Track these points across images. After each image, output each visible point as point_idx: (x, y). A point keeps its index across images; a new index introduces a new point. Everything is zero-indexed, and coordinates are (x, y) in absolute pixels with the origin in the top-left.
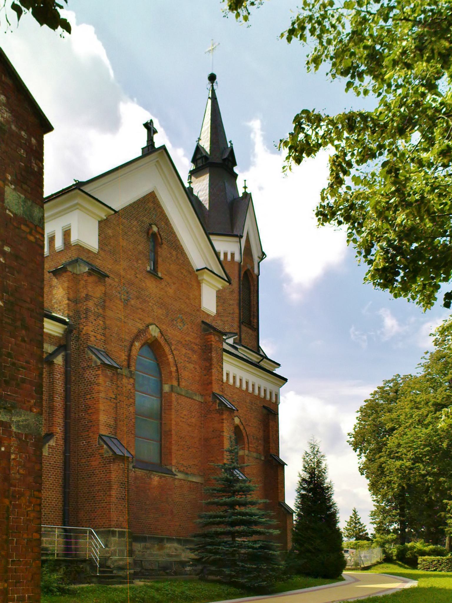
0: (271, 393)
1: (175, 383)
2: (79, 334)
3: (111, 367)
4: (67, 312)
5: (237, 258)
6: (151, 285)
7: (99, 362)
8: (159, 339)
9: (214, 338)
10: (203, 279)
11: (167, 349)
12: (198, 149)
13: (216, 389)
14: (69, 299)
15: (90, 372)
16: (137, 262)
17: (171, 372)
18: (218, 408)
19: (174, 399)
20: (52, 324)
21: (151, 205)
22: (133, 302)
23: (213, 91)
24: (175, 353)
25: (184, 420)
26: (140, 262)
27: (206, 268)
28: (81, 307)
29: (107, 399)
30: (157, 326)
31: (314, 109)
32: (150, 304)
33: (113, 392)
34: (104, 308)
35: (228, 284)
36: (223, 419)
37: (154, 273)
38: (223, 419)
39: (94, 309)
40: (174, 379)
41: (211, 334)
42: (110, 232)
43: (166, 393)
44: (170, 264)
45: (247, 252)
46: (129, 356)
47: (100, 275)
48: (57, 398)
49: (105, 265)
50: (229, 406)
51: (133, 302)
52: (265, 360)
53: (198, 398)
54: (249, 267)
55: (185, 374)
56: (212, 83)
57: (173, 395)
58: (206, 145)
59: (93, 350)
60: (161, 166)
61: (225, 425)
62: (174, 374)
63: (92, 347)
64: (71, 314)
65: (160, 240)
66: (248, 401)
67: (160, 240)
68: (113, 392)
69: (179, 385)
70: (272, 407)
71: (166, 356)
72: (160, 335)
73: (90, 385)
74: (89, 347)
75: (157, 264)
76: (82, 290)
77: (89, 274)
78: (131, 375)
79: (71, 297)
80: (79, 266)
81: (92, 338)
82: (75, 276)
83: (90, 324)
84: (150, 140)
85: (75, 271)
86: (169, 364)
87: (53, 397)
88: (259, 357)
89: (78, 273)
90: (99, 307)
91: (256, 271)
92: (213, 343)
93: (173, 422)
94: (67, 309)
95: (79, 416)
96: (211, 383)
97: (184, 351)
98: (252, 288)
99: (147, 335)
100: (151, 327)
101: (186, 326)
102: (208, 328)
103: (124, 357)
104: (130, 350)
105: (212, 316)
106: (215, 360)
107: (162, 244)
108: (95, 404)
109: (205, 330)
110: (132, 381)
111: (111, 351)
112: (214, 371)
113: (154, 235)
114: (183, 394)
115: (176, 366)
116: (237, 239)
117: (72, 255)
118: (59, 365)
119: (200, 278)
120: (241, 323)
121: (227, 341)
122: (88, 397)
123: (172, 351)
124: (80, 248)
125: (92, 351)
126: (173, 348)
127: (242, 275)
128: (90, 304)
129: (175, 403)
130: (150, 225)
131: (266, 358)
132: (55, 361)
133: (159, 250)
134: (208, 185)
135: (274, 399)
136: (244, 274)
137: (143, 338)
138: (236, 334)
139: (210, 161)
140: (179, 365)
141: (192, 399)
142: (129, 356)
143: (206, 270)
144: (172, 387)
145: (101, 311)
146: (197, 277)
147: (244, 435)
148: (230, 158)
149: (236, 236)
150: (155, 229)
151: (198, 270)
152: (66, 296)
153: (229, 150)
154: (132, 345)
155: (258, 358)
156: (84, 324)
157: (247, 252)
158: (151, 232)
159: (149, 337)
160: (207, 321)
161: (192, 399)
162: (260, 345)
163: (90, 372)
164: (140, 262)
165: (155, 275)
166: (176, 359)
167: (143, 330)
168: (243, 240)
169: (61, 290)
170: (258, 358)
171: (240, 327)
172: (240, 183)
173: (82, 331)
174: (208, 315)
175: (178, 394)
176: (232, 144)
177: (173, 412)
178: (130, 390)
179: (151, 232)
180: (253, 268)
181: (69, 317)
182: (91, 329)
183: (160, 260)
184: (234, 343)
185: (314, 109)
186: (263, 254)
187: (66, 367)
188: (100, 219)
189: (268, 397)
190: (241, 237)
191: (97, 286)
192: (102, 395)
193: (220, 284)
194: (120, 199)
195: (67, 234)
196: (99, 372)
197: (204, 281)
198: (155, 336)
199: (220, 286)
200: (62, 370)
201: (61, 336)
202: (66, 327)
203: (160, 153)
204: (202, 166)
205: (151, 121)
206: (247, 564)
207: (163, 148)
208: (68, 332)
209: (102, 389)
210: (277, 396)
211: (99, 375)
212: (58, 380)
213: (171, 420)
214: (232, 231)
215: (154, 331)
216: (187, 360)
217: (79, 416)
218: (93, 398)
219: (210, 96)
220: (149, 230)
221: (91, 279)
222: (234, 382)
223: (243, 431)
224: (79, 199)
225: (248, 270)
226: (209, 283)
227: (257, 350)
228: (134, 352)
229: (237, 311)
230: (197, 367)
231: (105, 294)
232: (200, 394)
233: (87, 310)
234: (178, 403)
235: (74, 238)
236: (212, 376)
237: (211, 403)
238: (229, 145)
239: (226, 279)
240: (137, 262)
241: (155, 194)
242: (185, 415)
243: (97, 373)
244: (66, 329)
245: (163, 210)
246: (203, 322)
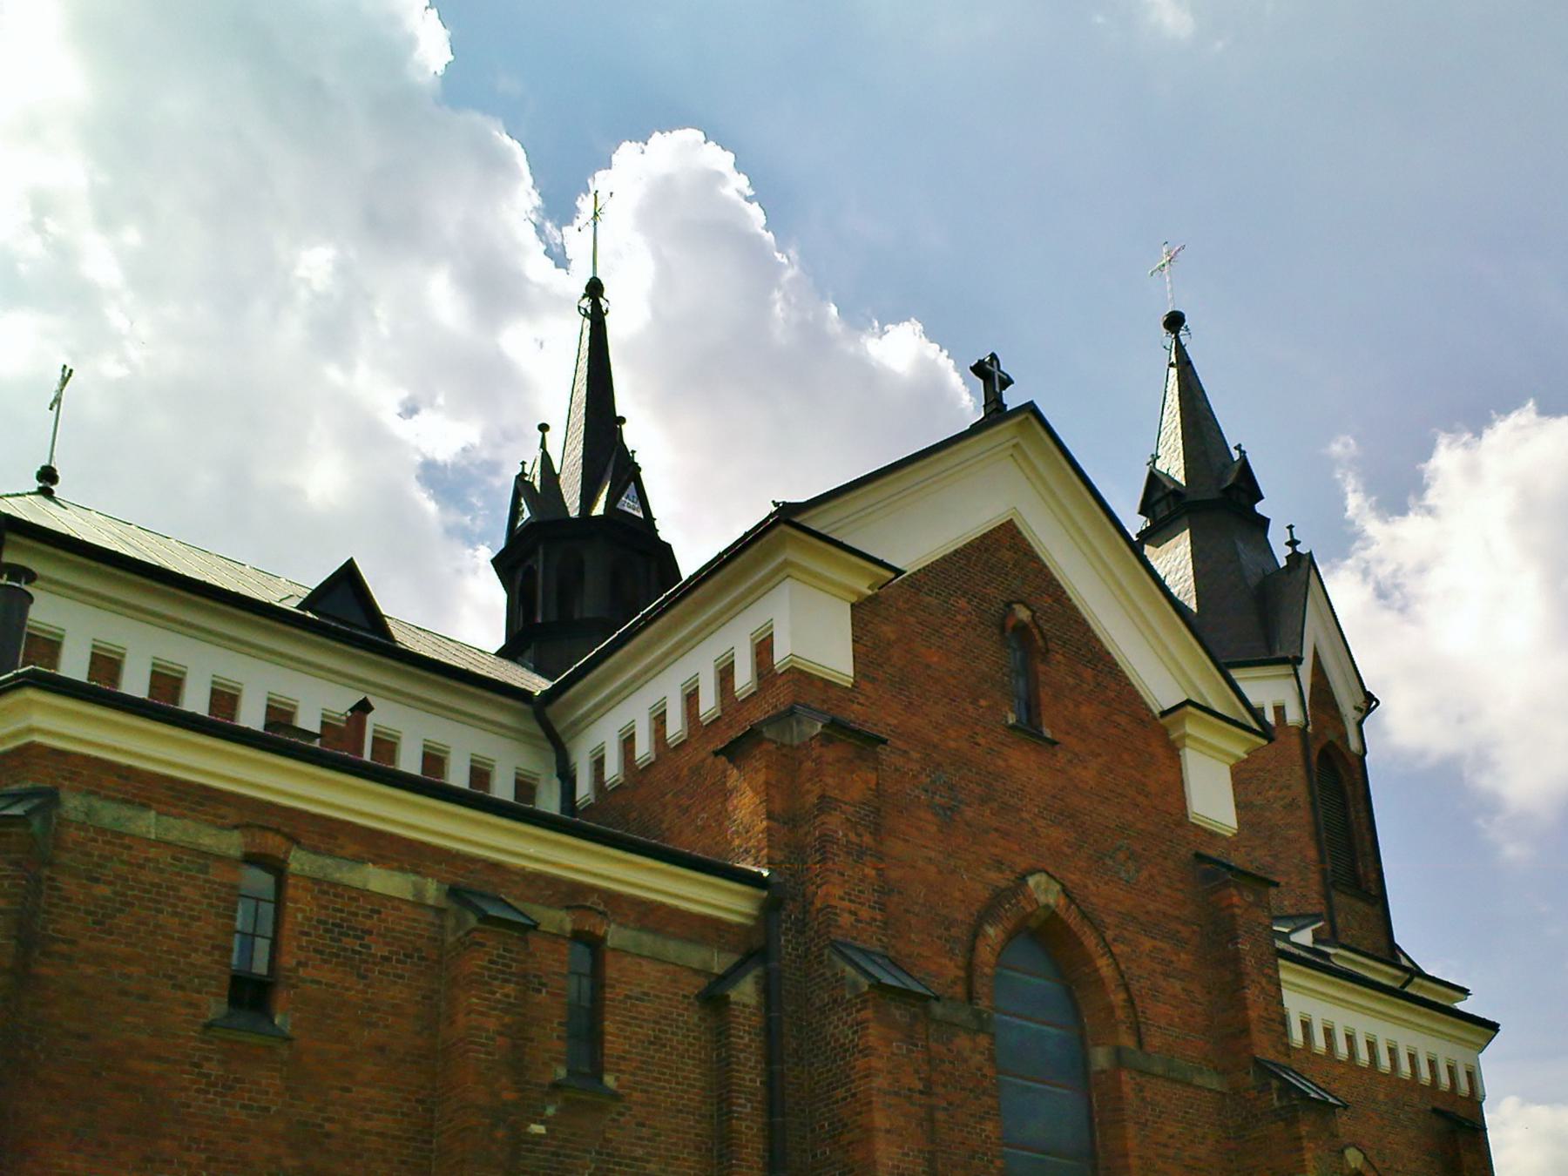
0: (1451, 1070)
1: (1127, 1041)
2: (806, 912)
3: (904, 994)
4: (765, 851)
5: (1294, 716)
6: (1022, 763)
7: (864, 984)
8: (1062, 914)
9: (1239, 899)
10: (1185, 736)
11: (1090, 941)
12: (1154, 480)
13: (1265, 1049)
14: (770, 816)
15: (840, 1019)
16: (975, 702)
17: (1110, 1009)
18: (1276, 1104)
19: (1126, 1089)
20: (730, 891)
21: (1006, 555)
22: (969, 813)
23: (1180, 349)
24: (1118, 949)
25: (1171, 1152)
26: (983, 703)
27: (1188, 702)
28: (806, 834)
29: (897, 1094)
30: (1051, 876)
32: (1024, 815)
33: (916, 1072)
34: (877, 830)
35: (1264, 742)
36: (1300, 1138)
37: (1029, 730)
38: (1300, 1138)
39: (846, 835)
40: (1123, 1028)
41: (1226, 884)
42: (889, 631)
43: (1103, 1071)
44: (1077, 705)
45: (1322, 697)
46: (970, 967)
47: (867, 742)
48: (740, 1105)
49: (880, 716)
50: (1313, 1095)
51: (969, 813)
52: (1416, 980)
53: (1213, 1082)
54: (1331, 735)
56: (1176, 332)
57: (1125, 1076)
58: (1173, 465)
59: (849, 952)
60: (1026, 457)
61: (1308, 1156)
63: (846, 945)
64: (779, 856)
65: (1041, 643)
66: (1381, 1097)
67: (1041, 643)
68: (916, 1072)
69: (1140, 1043)
70: (1462, 1112)
71: (1088, 960)
72: (1063, 901)
73: (843, 1058)
74: (834, 945)
75: (1038, 705)
76: (808, 785)
77: (826, 739)
78: (982, 1025)
79: (778, 806)
80: (799, 722)
81: (846, 919)
82: (784, 751)
83: (835, 878)
85: (787, 740)
86: (1100, 982)
87: (732, 1104)
88: (1399, 973)
89: (796, 742)
90: (860, 829)
91: (1354, 744)
92: (1237, 911)
93: (1133, 1161)
94: (764, 843)
95: (814, 1156)
96: (1245, 1031)
97: (1148, 944)
98: (1349, 789)
99: (1023, 903)
100: (1031, 881)
101: (1145, 874)
102: (1210, 867)
103: (952, 969)
104: (972, 949)
105: (1224, 837)
106: (1250, 963)
107: (1048, 651)
108: (859, 1113)
110: (983, 1041)
111: (909, 956)
112: (1251, 993)
113: (1022, 630)
114: (1159, 1069)
115: (1127, 989)
116: (1288, 669)
117: (781, 698)
118: (745, 1006)
119: (1174, 735)
120: (1329, 886)
121: (1295, 938)
122: (841, 1093)
123: (1106, 945)
124: (800, 677)
125: (841, 952)
126: (1109, 935)
127: (1314, 757)
128: (834, 822)
130: (1009, 605)
131: (1419, 973)
132: (734, 995)
133: (1041, 667)
134: (1189, 555)
135: (1464, 1087)
136: (1319, 757)
138: (1316, 917)
139: (1188, 499)
140: (1135, 986)
141: (1189, 1084)
142: (970, 967)
143: (1190, 709)
144: (1118, 1052)
145: (868, 839)
146: (1164, 732)
148: (1243, 485)
149: (1283, 661)
150: (1023, 614)
151: (1164, 713)
152: (762, 809)
153: (1237, 467)
154: (976, 933)
155: (1395, 978)
156: (819, 881)
157: (1322, 697)
158: (1010, 623)
159: (1029, 909)
160: (1213, 854)
161: (1189, 1084)
162: (1397, 941)
163: (840, 1019)
164: (983, 703)
165: (1032, 735)
166: (1123, 967)
167: (1009, 889)
168: (1305, 670)
169: (749, 793)
170: (1395, 978)
172: (1277, 539)
173: (812, 903)
174: (1213, 835)
175: (1142, 1072)
176: (1243, 453)
177: (1131, 1130)
178: (979, 1069)
179: (1010, 623)
180: (1344, 737)
181: (770, 864)
182: (840, 894)
183: (1045, 695)
184: (1316, 940)
186: (1370, 698)
187: (768, 1009)
188: (854, 599)
189: (1444, 1080)
190: (1298, 660)
191: (853, 772)
192: (879, 1082)
193: (1238, 746)
194: (915, 540)
195: (763, 648)
196: (868, 1013)
197: (1188, 742)
198: (1047, 906)
199: (1240, 752)
200: (757, 1021)
201: (749, 922)
202: (765, 894)
203: (1020, 423)
204: (1170, 515)
205: (993, 356)
207: (1030, 409)
208: (771, 908)
209: (876, 1063)
210: (1472, 1076)
211: (867, 1020)
212: (742, 1051)
213: (1126, 1155)
214: (1270, 648)
215: (1043, 891)
216: (1158, 968)
217: (814, 1156)
218: (854, 1095)
219: (1174, 360)
220: (1004, 617)
221: (830, 754)
224: (794, 552)
225: (1331, 744)
226: (1203, 742)
227: (1391, 953)
228: (985, 954)
229: (1312, 854)
231: (879, 792)
232: (1215, 1068)
233: (825, 840)
234: (1143, 1099)
235: (781, 654)
236: (1246, 1008)
237: (1254, 1093)
238: (1236, 455)
239: (1255, 726)
240: (975, 702)
241: (1015, 527)
242: (1172, 1137)
243: (860, 1016)
244: (766, 899)
245: (1045, 566)
246: (1200, 857)
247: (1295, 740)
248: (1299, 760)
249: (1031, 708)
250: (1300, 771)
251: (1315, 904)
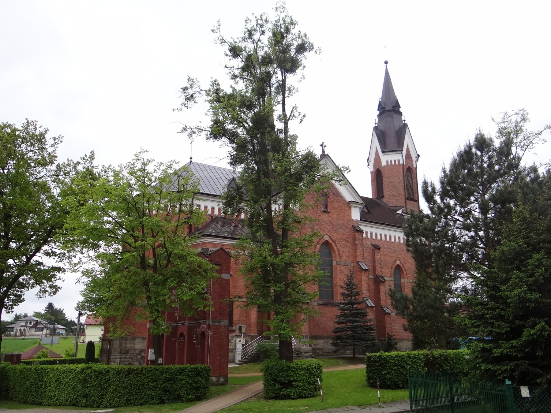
1: (338, 260)
11: (333, 244)
31: (389, 108)
37: (326, 212)
54: (409, 165)
55: (343, 254)
62: (337, 256)
84: (323, 151)
91: (415, 166)
93: (338, 279)
97: (343, 243)
109: (353, 230)
115: (338, 251)
127: (405, 171)
129: (338, 269)
137: (321, 243)
147: (404, 270)
157: (408, 156)
168: (404, 152)
171: (405, 202)
180: (412, 165)
184: (402, 212)
185: (389, 108)
186: (418, 155)
206: (536, 301)
222: (395, 240)
223: (403, 268)
230: (350, 249)
247: (401, 168)
248: (402, 172)
249: (326, 207)
250: (402, 175)
251: (403, 204)
